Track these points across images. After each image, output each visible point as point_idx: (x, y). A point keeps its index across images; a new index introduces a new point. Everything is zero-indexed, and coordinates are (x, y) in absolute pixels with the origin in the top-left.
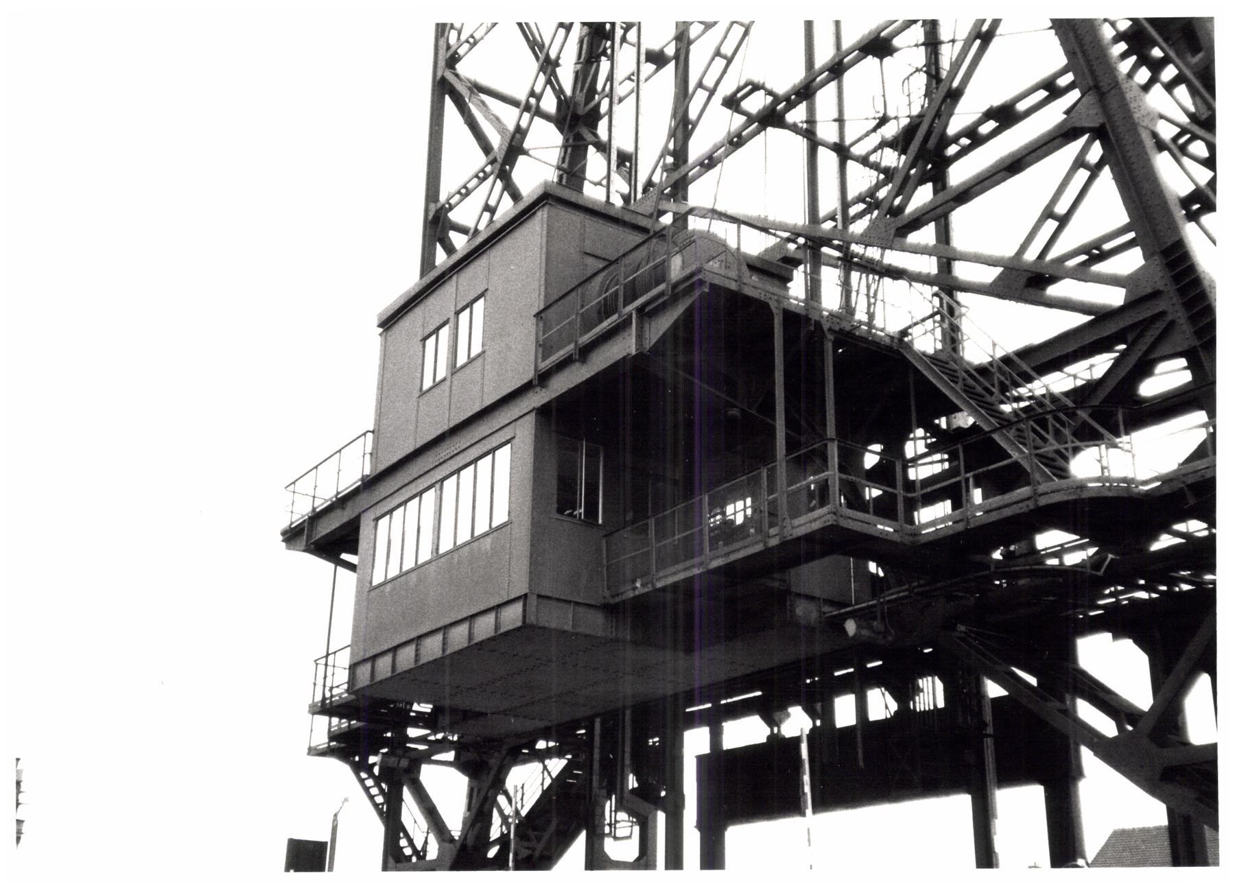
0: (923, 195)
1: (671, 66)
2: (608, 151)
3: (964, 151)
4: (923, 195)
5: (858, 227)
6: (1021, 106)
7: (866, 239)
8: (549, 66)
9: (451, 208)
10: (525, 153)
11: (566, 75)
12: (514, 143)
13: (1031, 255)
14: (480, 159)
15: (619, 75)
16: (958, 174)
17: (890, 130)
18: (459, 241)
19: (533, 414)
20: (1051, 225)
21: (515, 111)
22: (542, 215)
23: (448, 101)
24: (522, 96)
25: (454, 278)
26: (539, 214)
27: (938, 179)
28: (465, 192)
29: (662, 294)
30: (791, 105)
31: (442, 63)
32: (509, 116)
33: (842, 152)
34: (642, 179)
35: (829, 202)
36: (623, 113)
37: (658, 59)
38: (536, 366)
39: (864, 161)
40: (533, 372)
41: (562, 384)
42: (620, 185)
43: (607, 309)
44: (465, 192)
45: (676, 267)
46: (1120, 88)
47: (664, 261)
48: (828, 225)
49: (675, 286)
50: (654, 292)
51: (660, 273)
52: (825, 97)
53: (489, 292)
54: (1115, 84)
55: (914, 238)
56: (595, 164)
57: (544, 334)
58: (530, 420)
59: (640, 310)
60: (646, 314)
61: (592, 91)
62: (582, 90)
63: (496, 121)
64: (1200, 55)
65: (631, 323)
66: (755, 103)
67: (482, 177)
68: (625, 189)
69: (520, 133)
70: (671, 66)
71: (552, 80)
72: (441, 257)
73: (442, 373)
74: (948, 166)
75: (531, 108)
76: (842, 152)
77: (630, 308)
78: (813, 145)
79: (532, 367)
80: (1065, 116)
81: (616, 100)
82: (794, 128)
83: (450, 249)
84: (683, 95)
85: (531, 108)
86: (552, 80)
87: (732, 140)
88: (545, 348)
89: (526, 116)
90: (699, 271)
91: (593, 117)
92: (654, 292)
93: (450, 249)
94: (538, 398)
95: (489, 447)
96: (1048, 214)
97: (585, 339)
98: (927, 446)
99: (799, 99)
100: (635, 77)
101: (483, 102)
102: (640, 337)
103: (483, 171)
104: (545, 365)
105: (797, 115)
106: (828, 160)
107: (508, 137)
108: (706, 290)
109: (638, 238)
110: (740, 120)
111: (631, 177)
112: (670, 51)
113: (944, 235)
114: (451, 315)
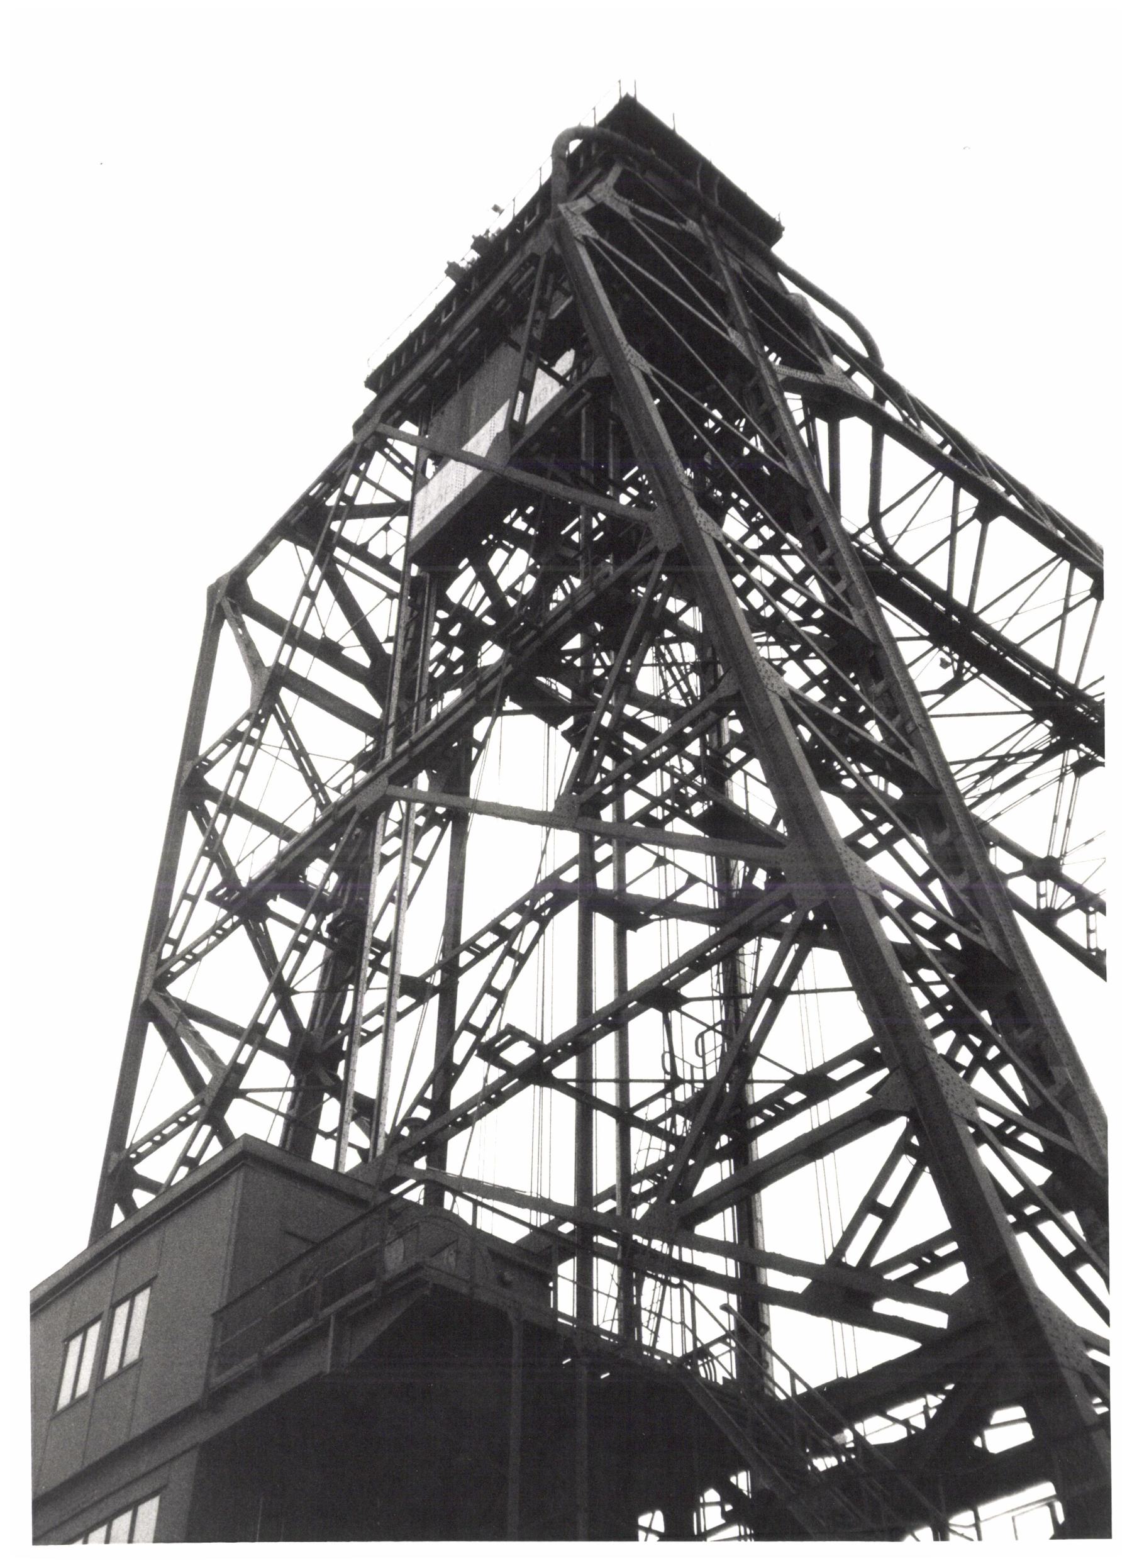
0: (714, 1175)
1: (434, 1002)
2: (342, 1095)
3: (769, 1124)
4: (714, 1175)
5: (640, 1212)
6: (837, 1075)
7: (648, 1227)
8: (282, 991)
9: (140, 1157)
10: (242, 1094)
11: (304, 1006)
12: (227, 1084)
13: (852, 1257)
14: (186, 1095)
15: (367, 1006)
16: (766, 1145)
17: (683, 1093)
18: (142, 1198)
19: (195, 1454)
20: (872, 1223)
21: (233, 1043)
22: (237, 1179)
23: (151, 1028)
24: (244, 1023)
25: (116, 1260)
26: (234, 1178)
27: (740, 1151)
28: (158, 1138)
29: (369, 1295)
30: (558, 1060)
31: (148, 983)
32: (225, 1047)
33: (625, 1117)
34: (387, 1127)
35: (605, 1176)
36: (367, 1057)
37: (417, 988)
38: (208, 1376)
39: (651, 1127)
40: (200, 1390)
41: (239, 1409)
42: (357, 1135)
43: (305, 1309)
44: (158, 1138)
45: (395, 1258)
46: (930, 1068)
47: (374, 1252)
48: (605, 1207)
49: (389, 1284)
50: (359, 1292)
51: (370, 1268)
52: (604, 1050)
53: (158, 1280)
54: (926, 1064)
55: (703, 1229)
56: (330, 1112)
57: (223, 1339)
58: (193, 1457)
59: (340, 1315)
60: (350, 1320)
61: (334, 1024)
62: (321, 1024)
63: (211, 1057)
64: (1029, 1031)
65: (327, 1336)
66: (518, 1053)
67: (182, 1120)
68: (365, 1143)
69: (238, 1071)
70: (434, 1002)
71: (286, 1006)
72: (118, 1216)
73: (83, 1387)
74: (755, 1138)
75: (255, 1035)
76: (625, 1117)
77: (328, 1311)
78: (587, 1104)
79: (202, 1382)
80: (870, 1097)
81: (357, 1039)
82: (561, 1085)
83: (129, 1208)
84: (447, 1034)
85: (255, 1035)
86: (286, 1006)
87: (694, 961)
88: (221, 1356)
89: (248, 1049)
90: (418, 1267)
91: (335, 1054)
92: (359, 1292)
93: (129, 1208)
94: (201, 1432)
95: (131, 1499)
96: (870, 1205)
97: (272, 1348)
98: (724, 1514)
99: (607, 1029)
100: (385, 1010)
101: (196, 1034)
102: (337, 1351)
103: (184, 1112)
104: (218, 1380)
105: (567, 1070)
106: (605, 1127)
107: (222, 1075)
108: (427, 1292)
109: (352, 1213)
110: (496, 1073)
111: (371, 1126)
112: (436, 980)
113: (748, 1224)
114: (106, 1307)
